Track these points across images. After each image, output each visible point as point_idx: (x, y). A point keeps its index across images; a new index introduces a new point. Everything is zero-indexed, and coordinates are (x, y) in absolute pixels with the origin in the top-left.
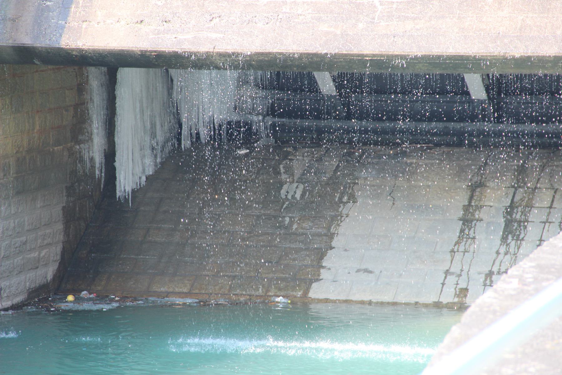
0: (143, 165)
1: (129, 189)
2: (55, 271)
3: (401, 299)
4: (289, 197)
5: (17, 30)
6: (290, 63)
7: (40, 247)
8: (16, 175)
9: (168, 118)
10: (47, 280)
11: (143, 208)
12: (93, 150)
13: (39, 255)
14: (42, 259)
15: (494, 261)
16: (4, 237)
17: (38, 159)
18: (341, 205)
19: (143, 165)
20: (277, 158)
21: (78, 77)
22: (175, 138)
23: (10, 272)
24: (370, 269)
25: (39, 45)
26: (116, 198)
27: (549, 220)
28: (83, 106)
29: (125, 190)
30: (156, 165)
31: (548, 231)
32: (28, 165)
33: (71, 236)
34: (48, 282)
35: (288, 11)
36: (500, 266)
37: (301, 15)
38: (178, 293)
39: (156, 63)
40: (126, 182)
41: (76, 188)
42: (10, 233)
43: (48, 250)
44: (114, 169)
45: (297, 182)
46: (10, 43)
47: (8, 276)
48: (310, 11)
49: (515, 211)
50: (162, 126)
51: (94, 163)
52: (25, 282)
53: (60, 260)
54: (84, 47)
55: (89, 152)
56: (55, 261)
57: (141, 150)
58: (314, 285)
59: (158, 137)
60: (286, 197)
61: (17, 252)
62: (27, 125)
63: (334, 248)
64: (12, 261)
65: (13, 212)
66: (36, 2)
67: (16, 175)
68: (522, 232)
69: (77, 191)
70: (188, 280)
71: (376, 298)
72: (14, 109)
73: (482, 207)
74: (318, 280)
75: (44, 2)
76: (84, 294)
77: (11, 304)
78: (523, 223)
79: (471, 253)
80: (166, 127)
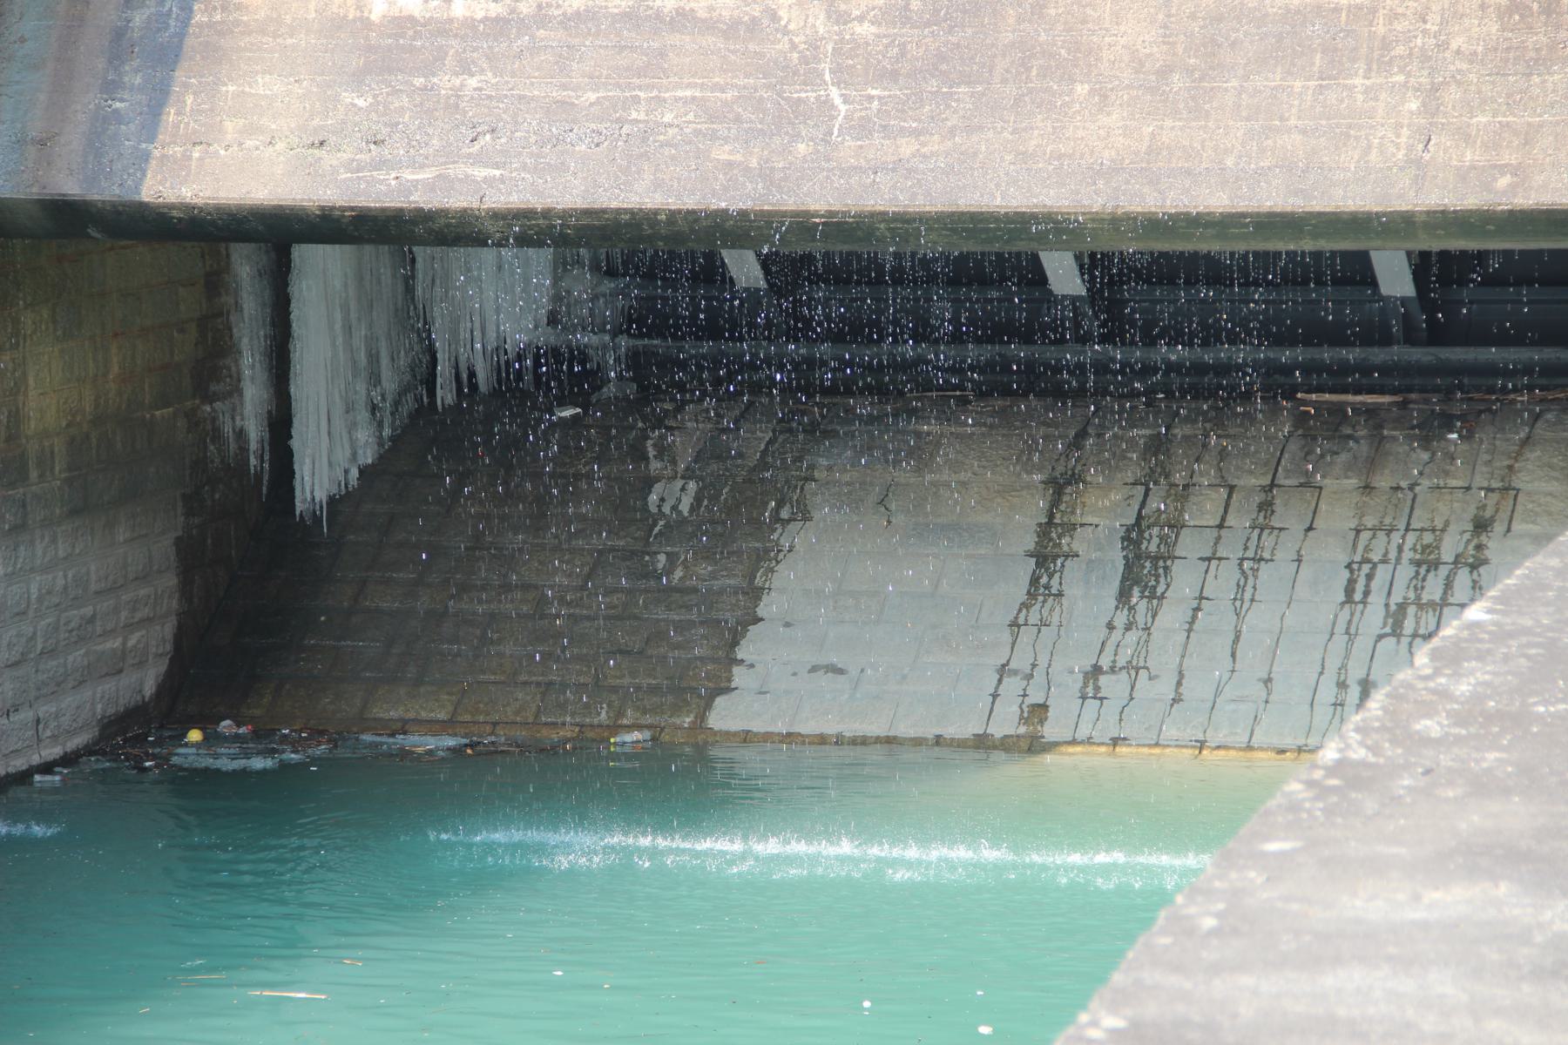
0: (353, 442)
1: (321, 495)
2: (161, 677)
3: (904, 730)
4: (666, 509)
5: (49, 164)
6: (649, 232)
7: (126, 626)
8: (67, 475)
9: (407, 341)
10: (143, 697)
11: (352, 537)
12: (242, 415)
13: (124, 644)
14: (130, 652)
15: (1103, 644)
16: (44, 608)
17: (118, 438)
18: (778, 525)
19: (353, 442)
20: (640, 425)
21: (207, 257)
22: (421, 385)
23: (58, 684)
24: (839, 666)
25: (96, 197)
26: (295, 515)
27: (1218, 555)
28: (219, 320)
29: (313, 499)
30: (380, 444)
31: (1216, 577)
32: (94, 451)
33: (196, 600)
34: (147, 699)
35: (642, 116)
36: (1115, 655)
37: (671, 126)
38: (427, 721)
39: (356, 234)
40: (316, 481)
41: (206, 496)
42: (56, 600)
43: (144, 632)
44: (289, 454)
45: (683, 477)
46: (35, 192)
47: (52, 693)
48: (691, 117)
49: (1146, 535)
50: (393, 359)
51: (247, 442)
52: (92, 704)
53: (172, 653)
54: (195, 201)
55: (233, 418)
56: (161, 655)
57: (347, 412)
58: (720, 701)
59: (385, 383)
60: (660, 510)
61: (73, 640)
62: (91, 364)
63: (762, 619)
64: (62, 661)
65: (61, 554)
66: (90, 103)
67: (67, 475)
68: (1162, 580)
69: (209, 503)
70: (448, 694)
71: (851, 728)
72: (59, 333)
73: (1073, 527)
74: (728, 690)
75: (110, 102)
76: (226, 726)
77: (61, 753)
78: (1163, 559)
79: (1054, 627)
80: (403, 361)
